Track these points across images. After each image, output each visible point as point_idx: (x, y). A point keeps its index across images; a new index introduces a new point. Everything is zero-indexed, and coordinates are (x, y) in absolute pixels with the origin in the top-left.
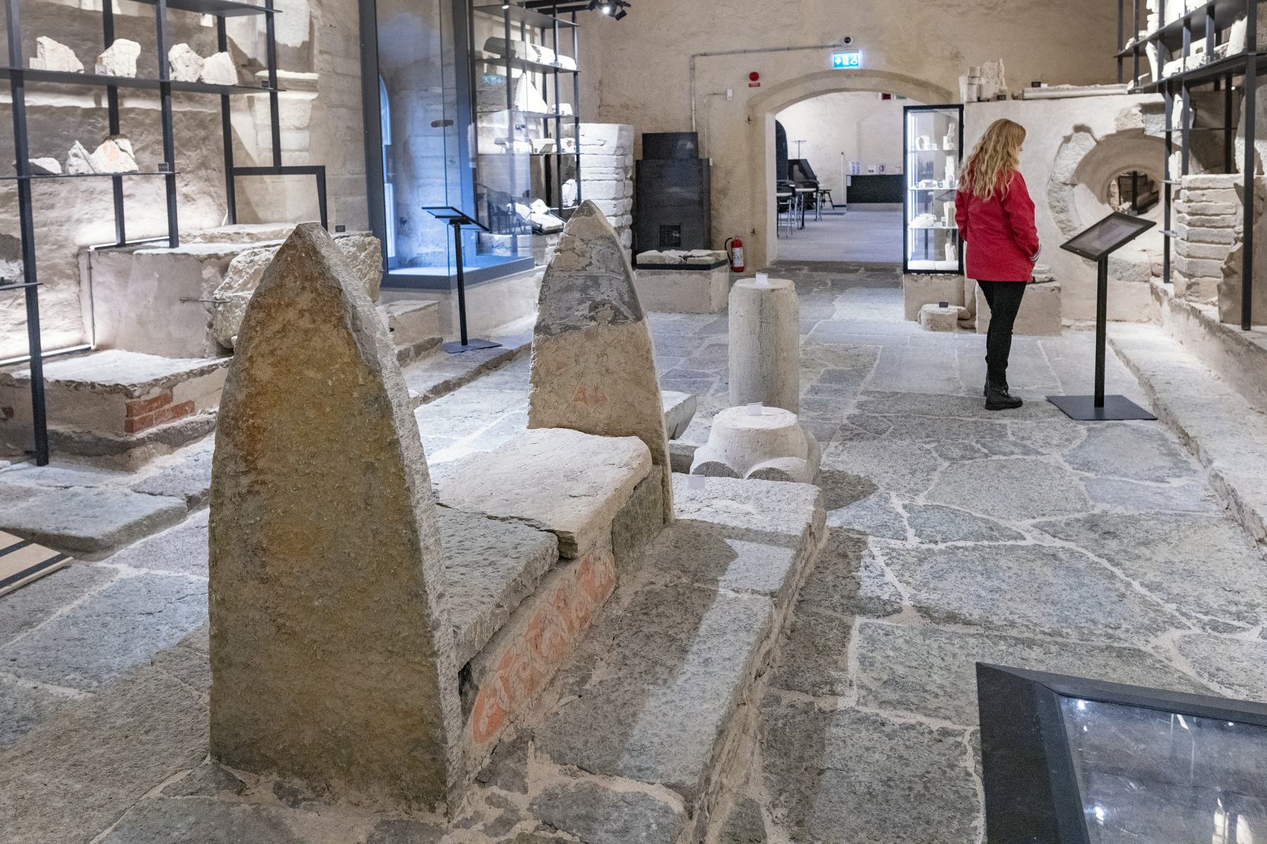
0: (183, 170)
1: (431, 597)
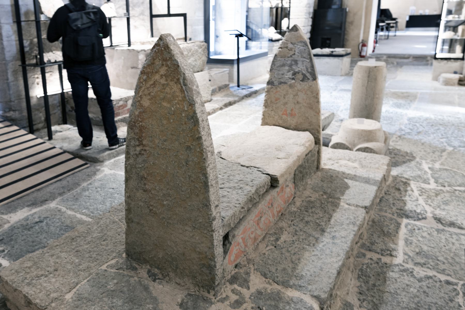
0: (134, 16)
1: (212, 207)
